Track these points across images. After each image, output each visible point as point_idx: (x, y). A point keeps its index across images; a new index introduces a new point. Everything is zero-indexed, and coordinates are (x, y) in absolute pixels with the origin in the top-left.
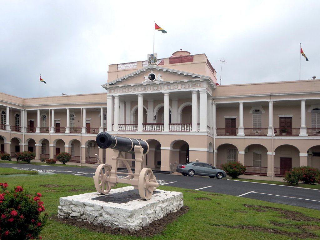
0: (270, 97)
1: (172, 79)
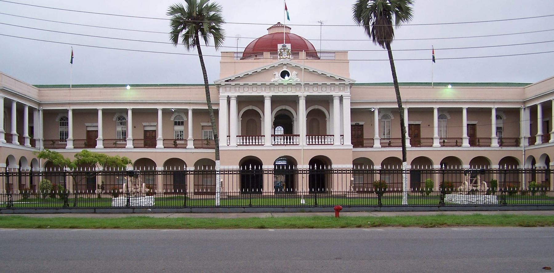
0: (494, 103)
1: (312, 80)
